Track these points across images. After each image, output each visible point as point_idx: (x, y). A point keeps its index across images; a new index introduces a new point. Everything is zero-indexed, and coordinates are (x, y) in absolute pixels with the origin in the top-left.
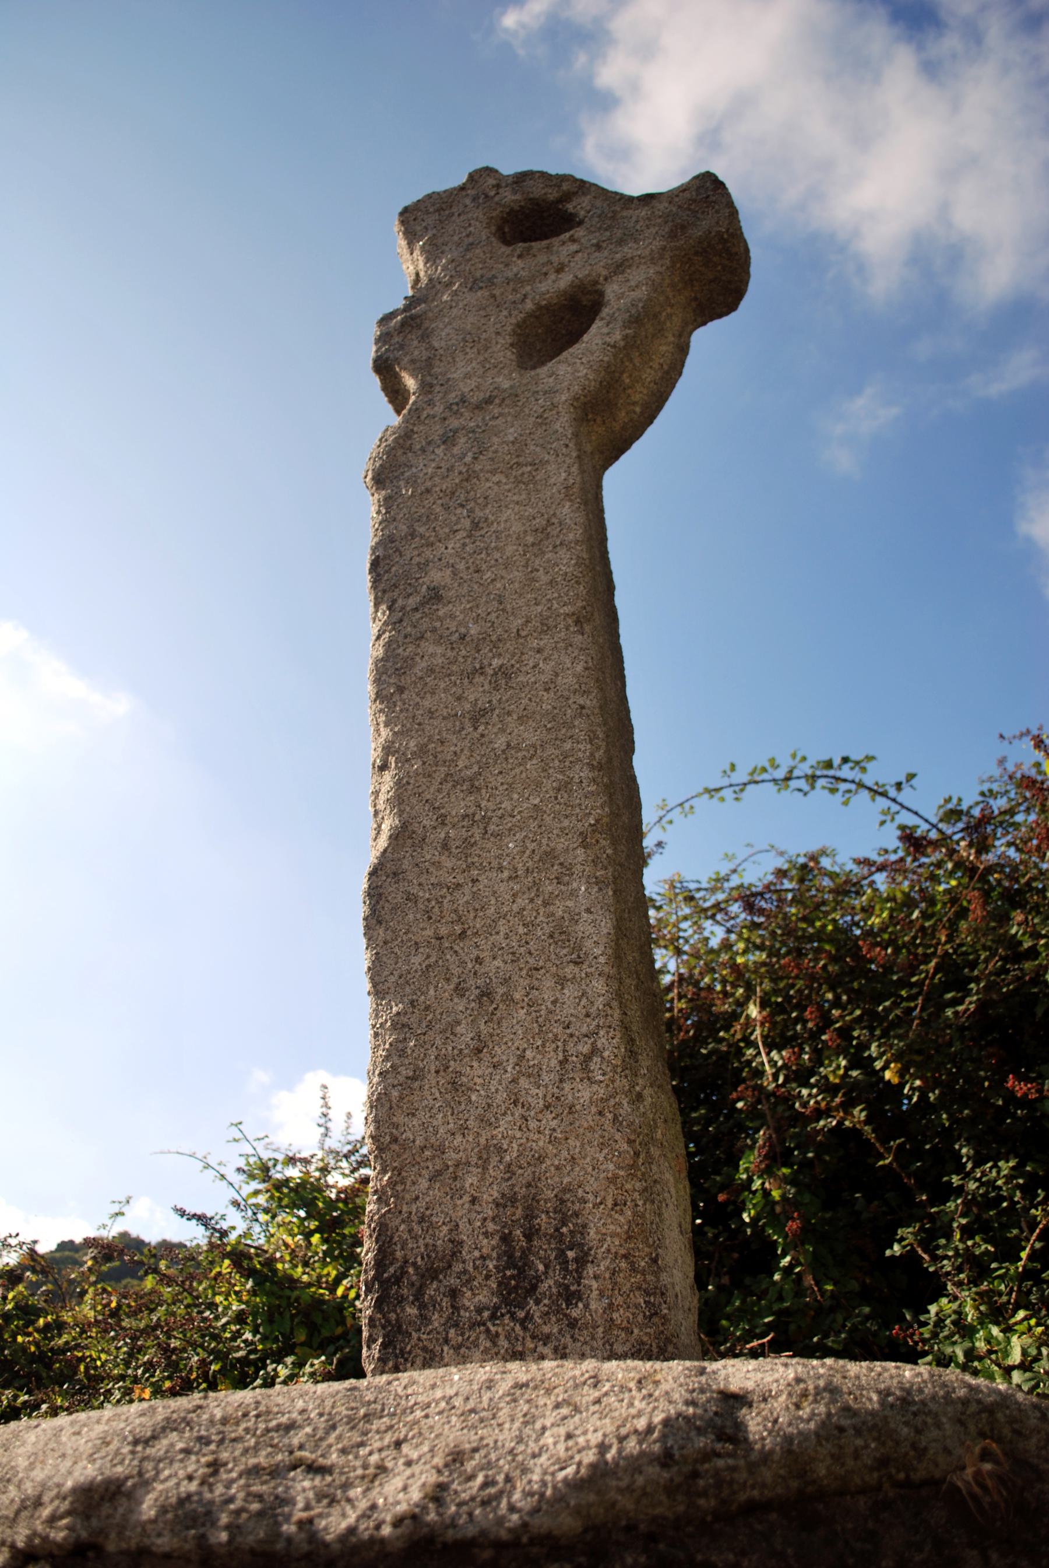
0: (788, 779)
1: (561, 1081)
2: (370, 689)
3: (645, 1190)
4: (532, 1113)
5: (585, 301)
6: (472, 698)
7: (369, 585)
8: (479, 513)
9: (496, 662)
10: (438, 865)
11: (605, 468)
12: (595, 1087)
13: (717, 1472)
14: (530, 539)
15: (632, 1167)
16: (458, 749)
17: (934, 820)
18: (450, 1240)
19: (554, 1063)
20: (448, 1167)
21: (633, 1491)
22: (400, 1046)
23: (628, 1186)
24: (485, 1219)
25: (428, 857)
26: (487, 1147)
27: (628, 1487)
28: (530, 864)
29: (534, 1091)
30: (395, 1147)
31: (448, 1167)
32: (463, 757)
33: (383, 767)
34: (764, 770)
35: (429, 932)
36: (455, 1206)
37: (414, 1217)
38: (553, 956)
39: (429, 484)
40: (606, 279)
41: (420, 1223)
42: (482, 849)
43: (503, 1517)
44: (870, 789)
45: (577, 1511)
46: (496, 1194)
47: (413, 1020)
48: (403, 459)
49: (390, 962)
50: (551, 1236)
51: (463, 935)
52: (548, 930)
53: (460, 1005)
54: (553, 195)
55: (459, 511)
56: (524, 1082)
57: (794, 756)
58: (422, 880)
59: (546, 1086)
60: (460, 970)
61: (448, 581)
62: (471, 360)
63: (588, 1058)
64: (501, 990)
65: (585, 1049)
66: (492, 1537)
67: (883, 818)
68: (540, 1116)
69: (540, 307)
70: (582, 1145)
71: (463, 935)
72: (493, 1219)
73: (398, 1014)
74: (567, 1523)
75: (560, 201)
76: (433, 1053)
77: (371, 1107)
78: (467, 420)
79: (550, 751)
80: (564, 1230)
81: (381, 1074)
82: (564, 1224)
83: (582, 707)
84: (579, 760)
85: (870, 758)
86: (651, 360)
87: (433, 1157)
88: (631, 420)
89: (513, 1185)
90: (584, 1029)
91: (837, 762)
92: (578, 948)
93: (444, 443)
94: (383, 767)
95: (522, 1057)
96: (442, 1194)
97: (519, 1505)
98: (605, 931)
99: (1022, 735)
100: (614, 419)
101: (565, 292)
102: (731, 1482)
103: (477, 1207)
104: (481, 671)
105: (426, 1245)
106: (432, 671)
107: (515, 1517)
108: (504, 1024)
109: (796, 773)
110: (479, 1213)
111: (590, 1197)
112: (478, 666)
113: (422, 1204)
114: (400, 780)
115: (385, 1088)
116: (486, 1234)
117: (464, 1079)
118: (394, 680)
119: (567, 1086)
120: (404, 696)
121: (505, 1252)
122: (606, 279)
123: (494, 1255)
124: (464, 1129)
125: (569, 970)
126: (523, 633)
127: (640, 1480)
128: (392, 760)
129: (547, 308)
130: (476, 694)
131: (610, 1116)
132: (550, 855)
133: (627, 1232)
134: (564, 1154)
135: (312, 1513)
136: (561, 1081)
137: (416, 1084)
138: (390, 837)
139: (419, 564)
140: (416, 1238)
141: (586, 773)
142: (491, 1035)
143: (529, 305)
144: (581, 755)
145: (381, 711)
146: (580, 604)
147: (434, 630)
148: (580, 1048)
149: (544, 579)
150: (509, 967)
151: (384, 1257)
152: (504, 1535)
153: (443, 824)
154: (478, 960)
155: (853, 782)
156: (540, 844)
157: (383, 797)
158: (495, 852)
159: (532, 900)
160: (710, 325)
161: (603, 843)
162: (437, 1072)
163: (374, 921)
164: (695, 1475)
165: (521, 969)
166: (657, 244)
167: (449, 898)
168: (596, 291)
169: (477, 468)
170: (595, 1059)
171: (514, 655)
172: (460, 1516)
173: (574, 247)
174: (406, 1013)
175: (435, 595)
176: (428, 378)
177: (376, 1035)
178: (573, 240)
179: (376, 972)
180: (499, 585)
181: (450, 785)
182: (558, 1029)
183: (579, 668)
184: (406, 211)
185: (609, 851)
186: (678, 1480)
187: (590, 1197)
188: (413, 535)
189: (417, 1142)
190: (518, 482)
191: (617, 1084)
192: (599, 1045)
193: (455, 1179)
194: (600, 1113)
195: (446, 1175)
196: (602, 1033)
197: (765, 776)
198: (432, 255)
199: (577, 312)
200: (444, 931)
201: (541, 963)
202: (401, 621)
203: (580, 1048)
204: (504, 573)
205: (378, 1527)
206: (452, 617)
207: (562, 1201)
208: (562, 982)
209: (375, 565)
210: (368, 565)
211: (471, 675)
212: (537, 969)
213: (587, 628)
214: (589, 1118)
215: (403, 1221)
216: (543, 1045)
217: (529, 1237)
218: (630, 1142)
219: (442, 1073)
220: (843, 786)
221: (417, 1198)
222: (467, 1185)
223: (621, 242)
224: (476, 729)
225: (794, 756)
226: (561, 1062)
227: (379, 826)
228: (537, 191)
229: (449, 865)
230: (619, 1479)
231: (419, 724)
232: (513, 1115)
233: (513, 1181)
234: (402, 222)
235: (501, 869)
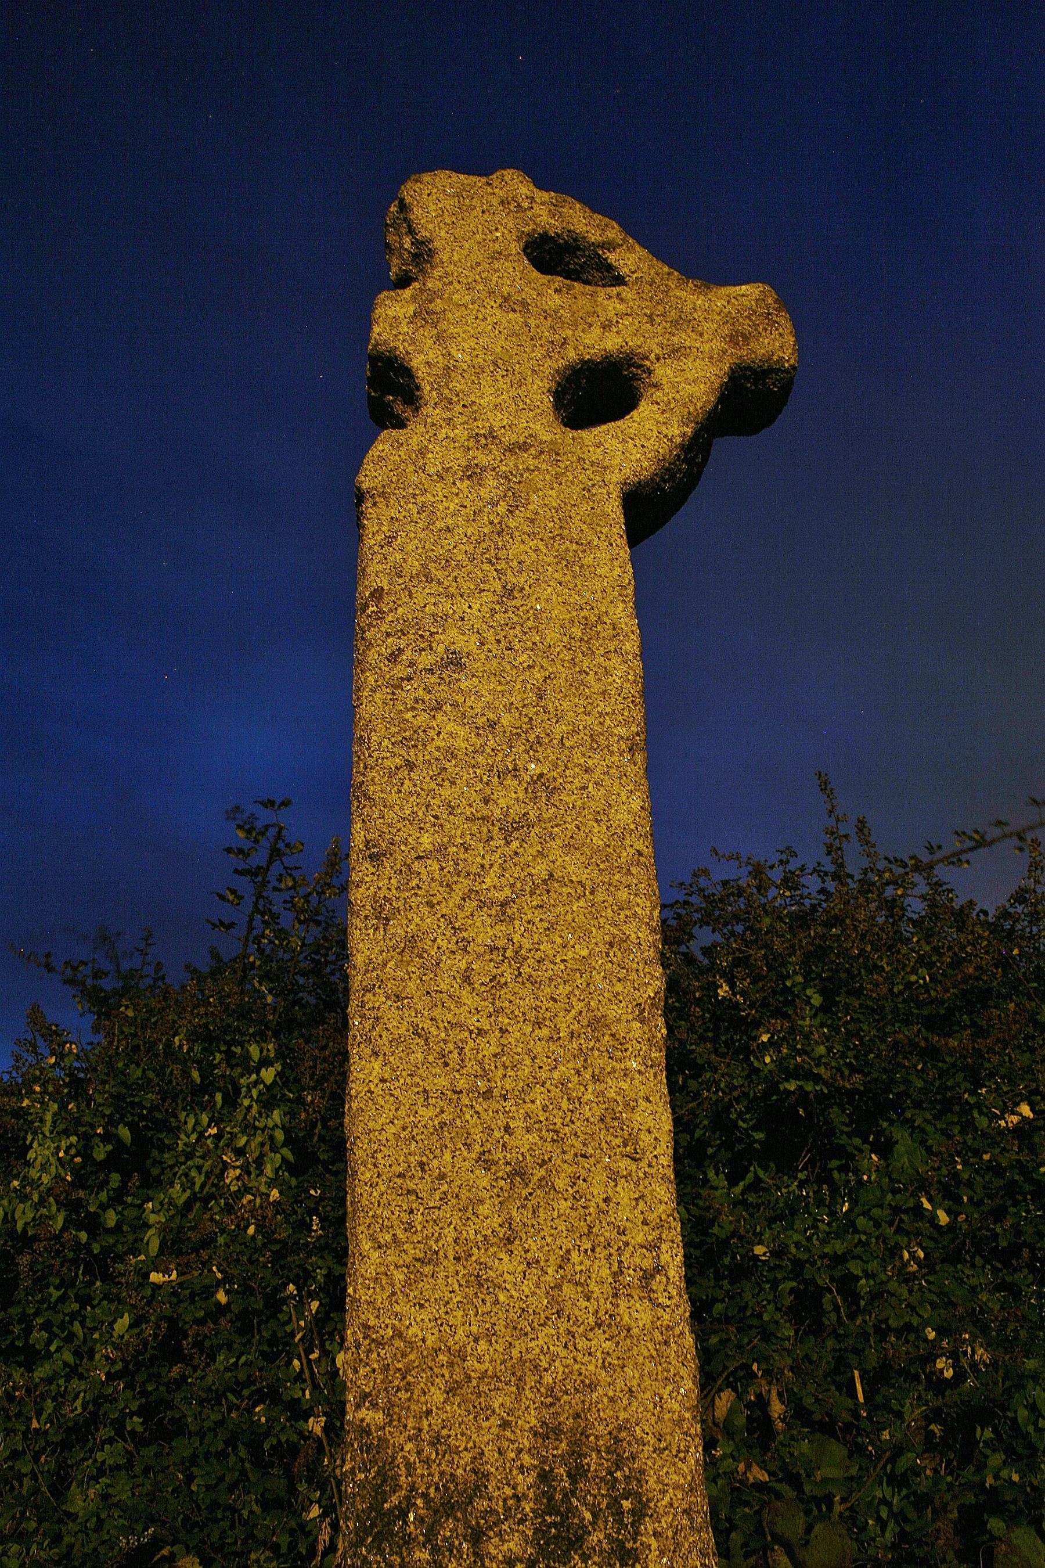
19: (605, 1272)
24: (520, 1451)
26: (522, 1361)
30: (398, 1343)
36: (481, 1428)
38: (604, 1146)
39: (450, 522)
46: (533, 1422)
51: (487, 1095)
56: (567, 1289)
70: (642, 1376)
75: (602, 246)
80: (618, 1474)
82: (618, 1468)
105: (442, 1473)
110: (512, 1442)
113: (435, 1421)
124: (490, 1335)
125: (624, 1164)
126: (567, 744)
130: (509, 798)
137: (427, 1270)
146: (634, 729)
162: (457, 1259)
165: (564, 1152)
169: (512, 524)
171: (555, 766)
175: (455, 661)
193: (479, 1395)
200: (462, 1084)
207: (617, 1440)
208: (614, 1177)
212: (584, 1156)
215: (410, 1439)
217: (573, 1478)
221: (429, 1412)
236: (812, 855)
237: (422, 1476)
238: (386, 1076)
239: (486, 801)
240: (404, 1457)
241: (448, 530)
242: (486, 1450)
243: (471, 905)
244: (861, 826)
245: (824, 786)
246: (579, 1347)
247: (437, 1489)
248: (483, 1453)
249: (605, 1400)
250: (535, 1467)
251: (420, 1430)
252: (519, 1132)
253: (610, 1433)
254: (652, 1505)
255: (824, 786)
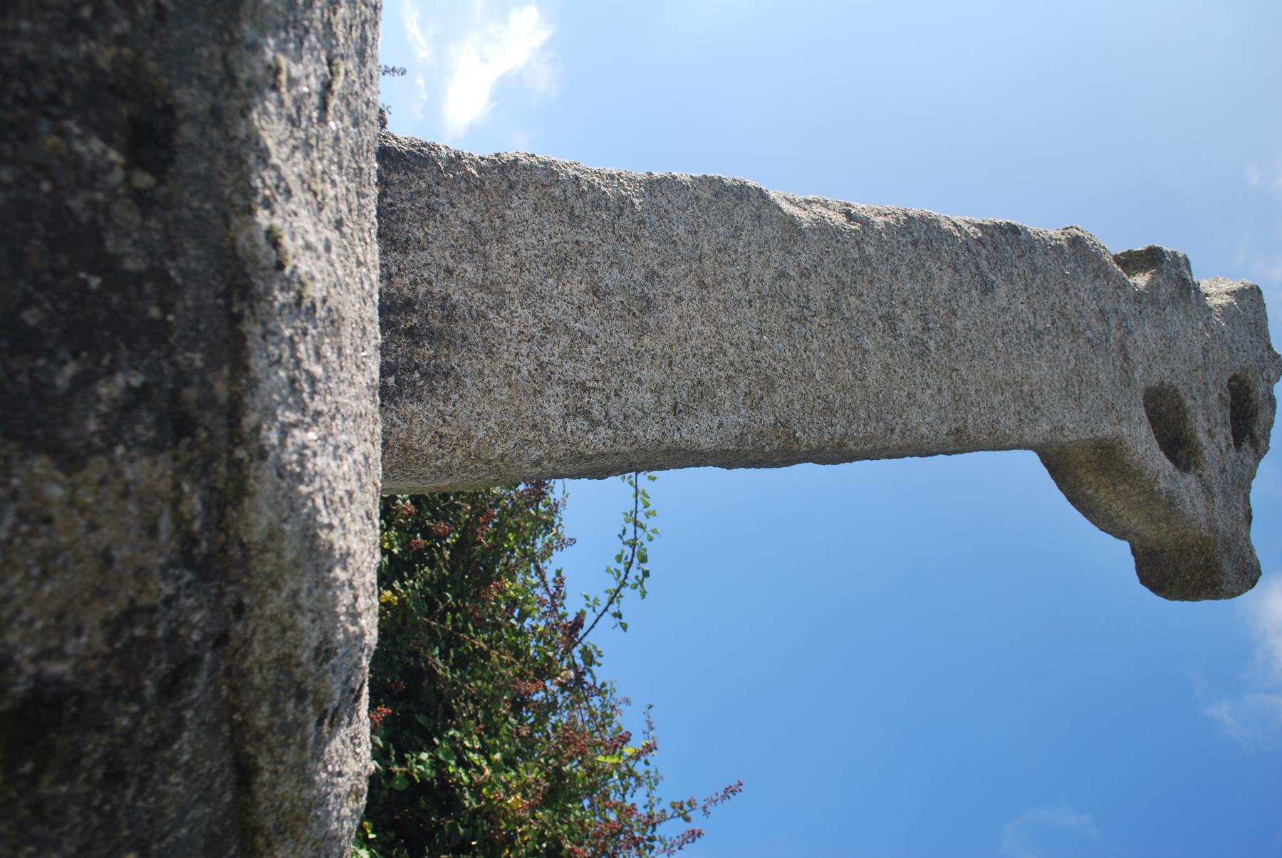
0: (636, 523)
1: (565, 382)
2: (914, 210)
3: (450, 467)
4: (535, 348)
5: (1182, 453)
6: (905, 316)
7: (998, 221)
8: (1047, 338)
9: (932, 344)
10: (766, 265)
11: (1039, 455)
12: (560, 422)
13: (301, 725)
14: (1026, 388)
15: (478, 457)
16: (865, 298)
17: (584, 641)
18: (408, 240)
19: (583, 376)
20: (483, 245)
21: (292, 614)
22: (602, 203)
23: (459, 451)
24: (430, 283)
25: (774, 255)
26: (502, 292)
27: (299, 607)
28: (764, 365)
29: (557, 351)
30: (505, 185)
31: (483, 245)
32: (858, 302)
33: (848, 214)
34: (647, 505)
35: (706, 248)
36: (444, 249)
37: (433, 200)
38: (681, 383)
39: (1072, 292)
40: (1200, 476)
41: (428, 205)
42: (778, 313)
43: (275, 418)
44: (618, 591)
45: (274, 535)
46: (455, 298)
47: (625, 221)
48: (1090, 269)
49: (680, 202)
50: (411, 359)
51: (702, 284)
52: (706, 379)
53: (639, 275)
54: (1258, 431)
55: (1049, 319)
56: (565, 340)
57: (654, 531)
58: (754, 247)
59: (561, 366)
60: (671, 278)
61: (997, 303)
62: (1156, 343)
63: (587, 414)
64: (652, 322)
65: (596, 413)
66: (247, 400)
67: (592, 599)
68: (532, 357)
69: (1185, 412)
70: (503, 403)
71: (702, 284)
72: (430, 293)
73: (633, 205)
74: (258, 518)
75: (1252, 436)
76: (595, 239)
77: (545, 163)
78: (1115, 334)
79: (860, 394)
80: (417, 375)
81: (577, 178)
82: (423, 375)
83: (892, 431)
84: (851, 424)
85: (644, 594)
86: (1130, 509)
87: (494, 229)
88: (1082, 485)
89: (465, 320)
90: (612, 412)
91: (645, 567)
92: (688, 410)
93: (1101, 311)
94: (848, 214)
95: (589, 341)
96: (456, 235)
97: (289, 441)
98: (702, 442)
99: (650, 723)
100: (1084, 473)
101: (1194, 437)
102: (285, 745)
103: (442, 275)
104: (926, 329)
105: (404, 211)
106: (929, 278)
107: (274, 437)
108: (619, 323)
109: (639, 531)
110: (437, 276)
111: (450, 408)
112: (930, 325)
113: (446, 210)
114: (841, 233)
115: (563, 182)
116: (414, 283)
117: (569, 272)
118: (921, 234)
119: (560, 389)
120: (909, 246)
121: (394, 303)
122: (1200, 476)
123: (393, 290)
124: (520, 267)
125: (668, 399)
126: (954, 375)
127: (304, 622)
128: (856, 227)
129: (1184, 418)
130: (909, 322)
131: (530, 437)
132: (771, 387)
133: (411, 447)
134: (495, 382)
135: (283, 89)
136: (565, 382)
137: (566, 218)
138: (792, 216)
139: (1012, 274)
140: (411, 199)
141: (840, 430)
142: (609, 307)
143: (1189, 403)
144: (855, 427)
145: (898, 219)
146: (972, 434)
147: (961, 284)
148: (596, 406)
149: (996, 400)
150: (673, 334)
151: (392, 159)
152: (250, 419)
153: (802, 275)
154: (679, 299)
155: (626, 577)
156: (780, 377)
157: (824, 211)
158: (776, 327)
159: (732, 364)
160: (1132, 558)
161: (776, 443)
162: (577, 243)
163: (717, 187)
164: (301, 696)
165: (671, 346)
166: (1220, 525)
167: (737, 274)
168: (1189, 465)
169: (1081, 341)
170: (586, 423)
171: (937, 363)
172: (277, 345)
173: (1223, 446)
174: (633, 214)
175: (987, 288)
176: (1145, 300)
177: (612, 177)
178: (1228, 447)
179: (668, 183)
180: (992, 353)
181: (835, 285)
182: (614, 384)
183: (923, 430)
184: (1260, 292)
185: (767, 449)
186: (298, 673)
187: (450, 408)
188: (1035, 271)
189: (508, 212)
190: (1068, 379)
191: (561, 446)
192: (601, 429)
193: (471, 252)
194: (535, 426)
195: (474, 243)
196: (610, 432)
197: (640, 505)
198: (1225, 310)
199: (1178, 445)
200: (708, 264)
201: (676, 370)
202: (969, 250)
203: (596, 406)
204: (1002, 360)
205: (267, 204)
206: (971, 303)
207: (447, 375)
208: (658, 391)
209: (1014, 229)
210: (1013, 223)
211: (922, 317)
212: (670, 364)
213: (951, 439)
214: (529, 413)
215: (429, 186)
216: (600, 366)
217: (410, 332)
218: (502, 456)
219: (576, 248)
220: (621, 567)
221: (453, 205)
222: (464, 265)
223: (1224, 492)
224: (880, 318)
225: (654, 531)
226: (583, 384)
227: (797, 205)
228: (1262, 417)
229: (767, 277)
230: (310, 594)
231: (887, 260)
232: (534, 324)
233: (469, 320)
234: (1252, 288)
235: (760, 333)
236: (666, 795)
237: (400, 193)
238: (701, 202)
239: (905, 303)
240: (413, 180)
241: (1067, 290)
242: (425, 253)
243: (834, 282)
244: (694, 835)
245: (730, 792)
246: (521, 345)
247: (391, 205)
248: (424, 250)
249: (480, 366)
250: (417, 297)
251: (438, 196)
252: (678, 309)
253: (453, 368)
254: (392, 406)
255: (730, 792)
